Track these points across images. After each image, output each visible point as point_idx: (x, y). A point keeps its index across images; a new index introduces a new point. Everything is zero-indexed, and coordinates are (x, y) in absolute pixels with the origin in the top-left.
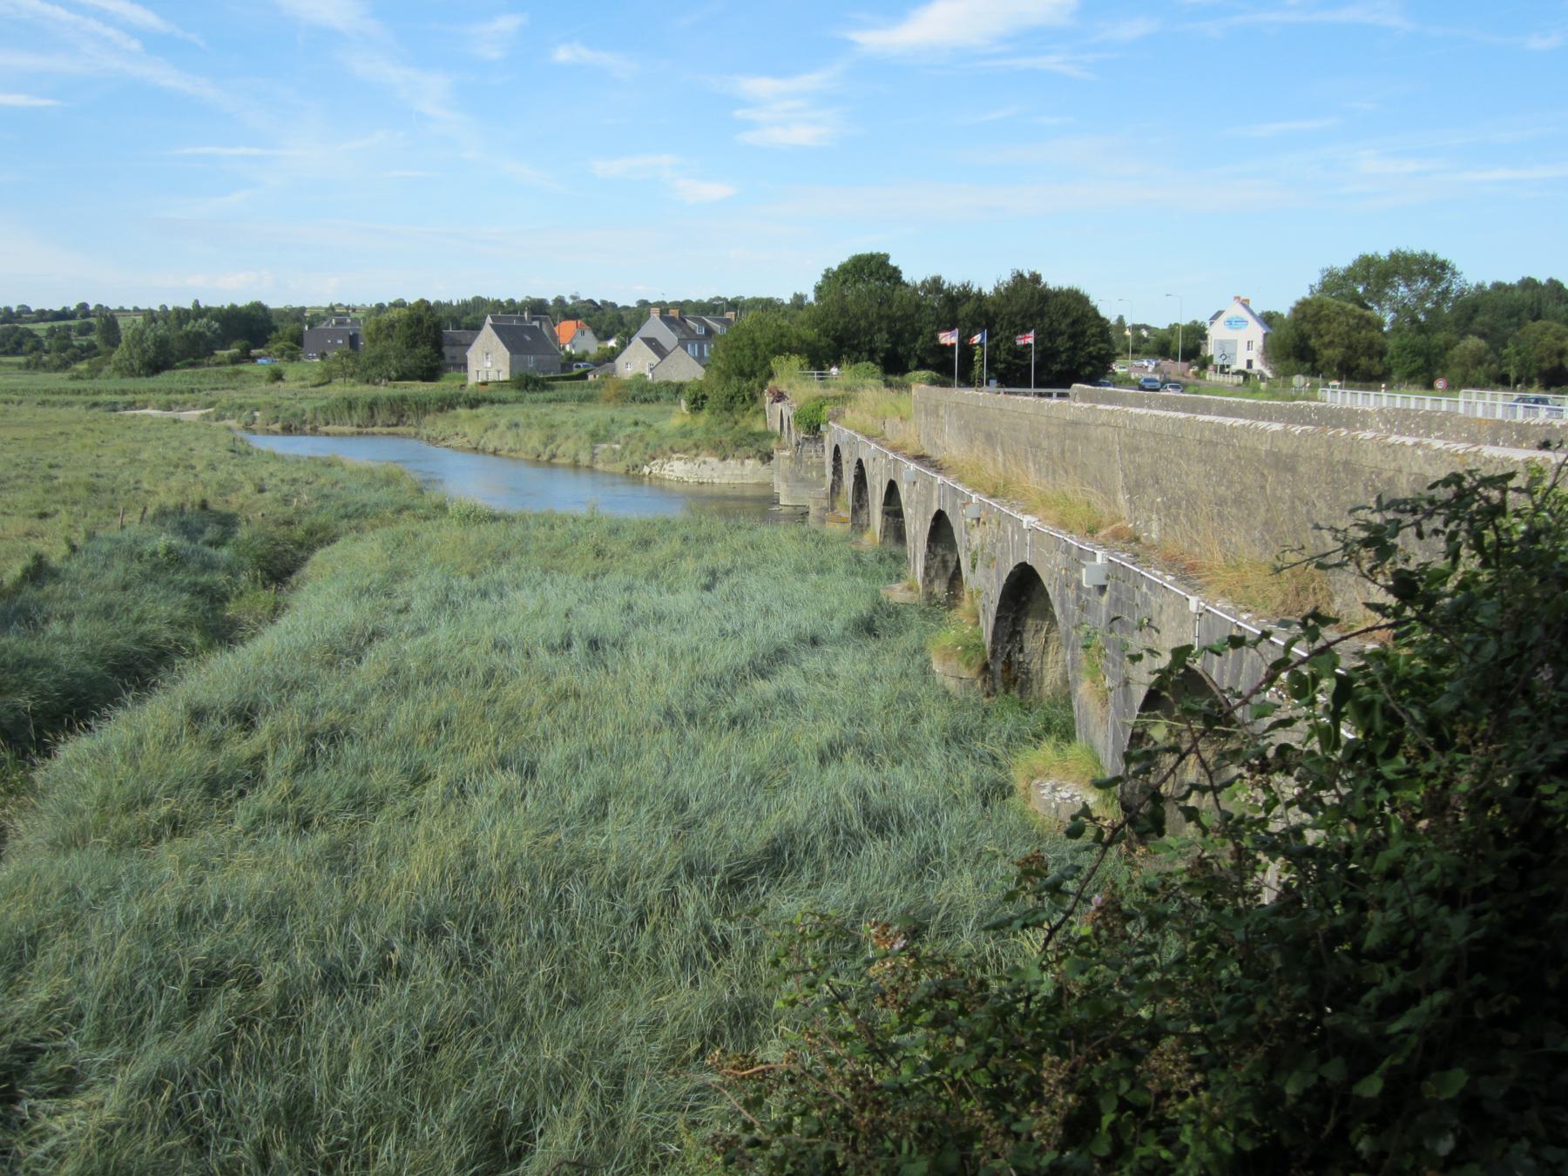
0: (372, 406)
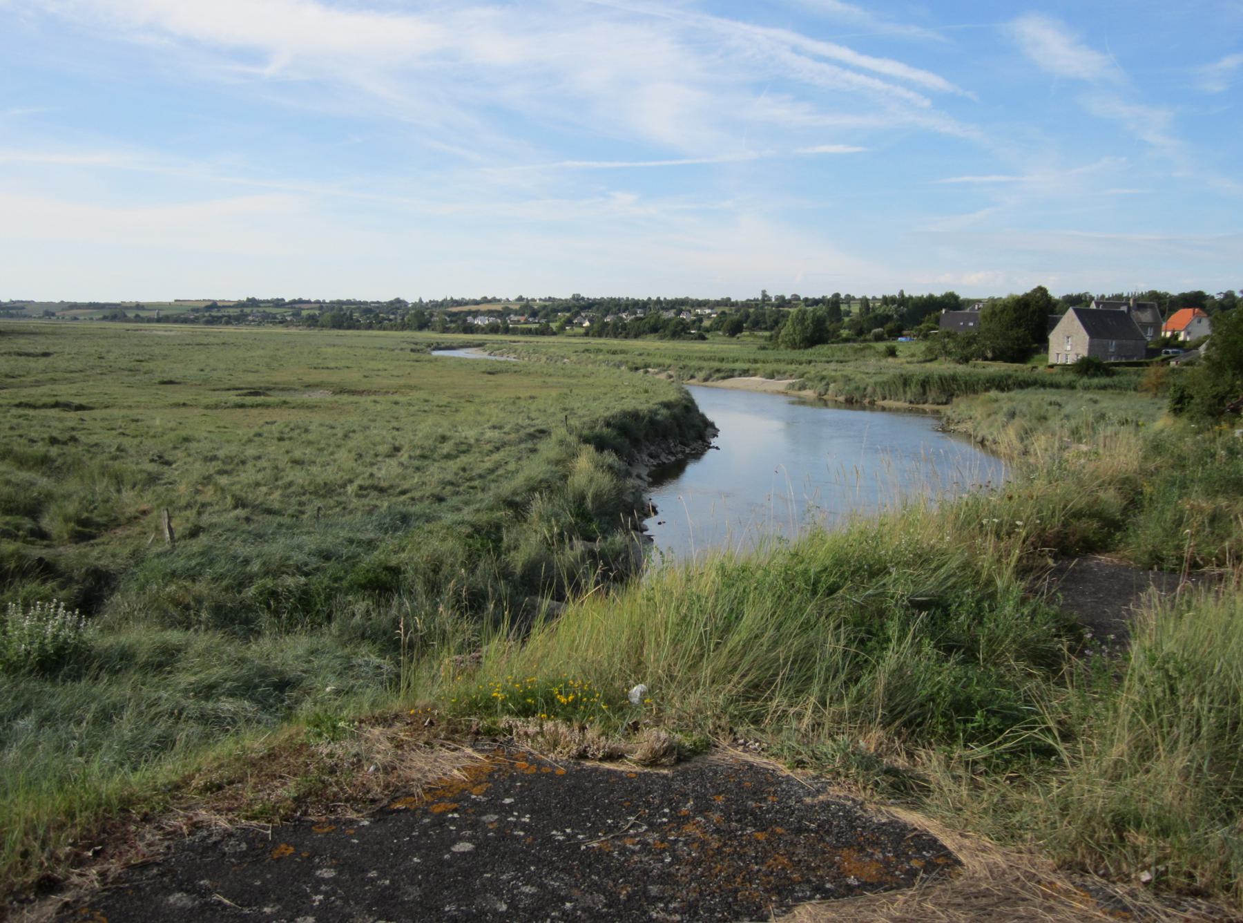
0: (925, 384)
